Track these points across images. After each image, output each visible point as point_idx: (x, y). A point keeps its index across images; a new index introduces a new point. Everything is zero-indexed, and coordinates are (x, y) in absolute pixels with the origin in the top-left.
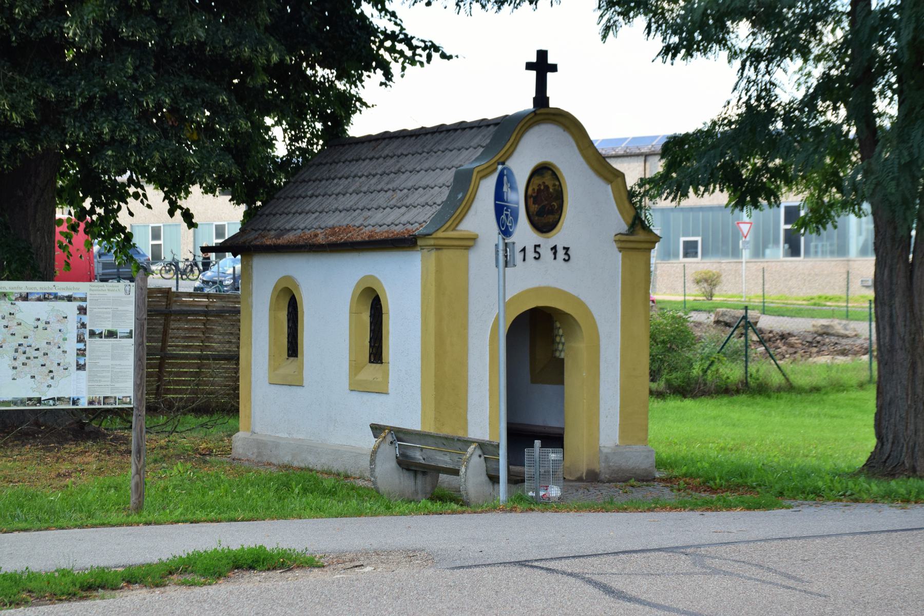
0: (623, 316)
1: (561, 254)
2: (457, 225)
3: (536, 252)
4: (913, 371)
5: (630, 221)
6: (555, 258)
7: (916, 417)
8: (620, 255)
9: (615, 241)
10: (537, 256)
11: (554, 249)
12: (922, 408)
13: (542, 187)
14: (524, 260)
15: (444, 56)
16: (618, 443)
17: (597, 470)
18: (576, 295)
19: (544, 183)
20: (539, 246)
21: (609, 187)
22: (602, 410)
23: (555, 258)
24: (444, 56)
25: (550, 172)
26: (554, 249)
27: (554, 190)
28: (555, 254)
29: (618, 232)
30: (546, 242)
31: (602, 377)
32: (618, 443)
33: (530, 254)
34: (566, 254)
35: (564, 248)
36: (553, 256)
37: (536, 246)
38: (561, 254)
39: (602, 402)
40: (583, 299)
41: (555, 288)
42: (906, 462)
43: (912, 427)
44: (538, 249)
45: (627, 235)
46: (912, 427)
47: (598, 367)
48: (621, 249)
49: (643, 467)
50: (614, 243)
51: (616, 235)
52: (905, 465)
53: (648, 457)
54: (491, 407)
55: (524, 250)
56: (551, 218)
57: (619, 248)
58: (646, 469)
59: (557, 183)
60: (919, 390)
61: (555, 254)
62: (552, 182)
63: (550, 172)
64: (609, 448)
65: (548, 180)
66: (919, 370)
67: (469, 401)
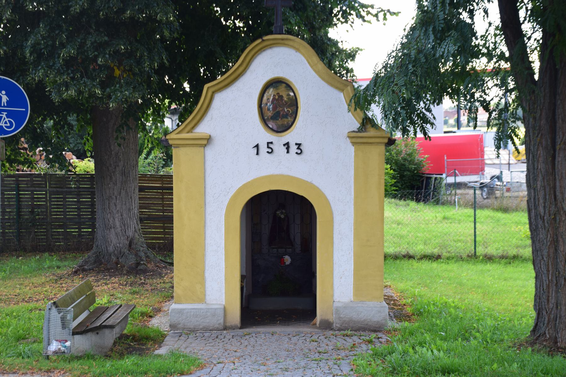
0: (356, 197)
1: (293, 149)
2: (193, 128)
3: (268, 147)
4: (556, 250)
5: (361, 121)
6: (288, 152)
7: (557, 292)
8: (352, 149)
9: (348, 137)
10: (270, 151)
11: (287, 145)
12: (563, 283)
13: (277, 97)
14: (257, 154)
15: (393, 14)
16: (352, 299)
17: (331, 320)
18: (309, 181)
19: (278, 94)
20: (272, 143)
21: (342, 94)
22: (335, 273)
23: (288, 152)
24: (393, 14)
25: (284, 85)
26: (287, 145)
27: (288, 98)
28: (288, 148)
29: (349, 131)
30: (279, 140)
31: (335, 246)
32: (352, 299)
33: (263, 149)
34: (298, 148)
35: (296, 144)
36: (286, 151)
37: (268, 143)
38: (293, 149)
39: (336, 267)
40: (316, 184)
41: (289, 176)
42: (547, 332)
43: (552, 300)
44: (271, 146)
45: (357, 132)
46: (552, 300)
47: (332, 238)
48: (354, 144)
49: (375, 319)
50: (348, 139)
51: (349, 132)
52: (546, 337)
53: (380, 312)
54: (226, 268)
55: (257, 146)
56: (286, 121)
57: (352, 143)
58: (378, 322)
59: (292, 94)
60: (561, 266)
61: (288, 148)
62: (287, 93)
63: (284, 85)
64: (342, 302)
65: (282, 91)
66: (561, 248)
67: (207, 262)
